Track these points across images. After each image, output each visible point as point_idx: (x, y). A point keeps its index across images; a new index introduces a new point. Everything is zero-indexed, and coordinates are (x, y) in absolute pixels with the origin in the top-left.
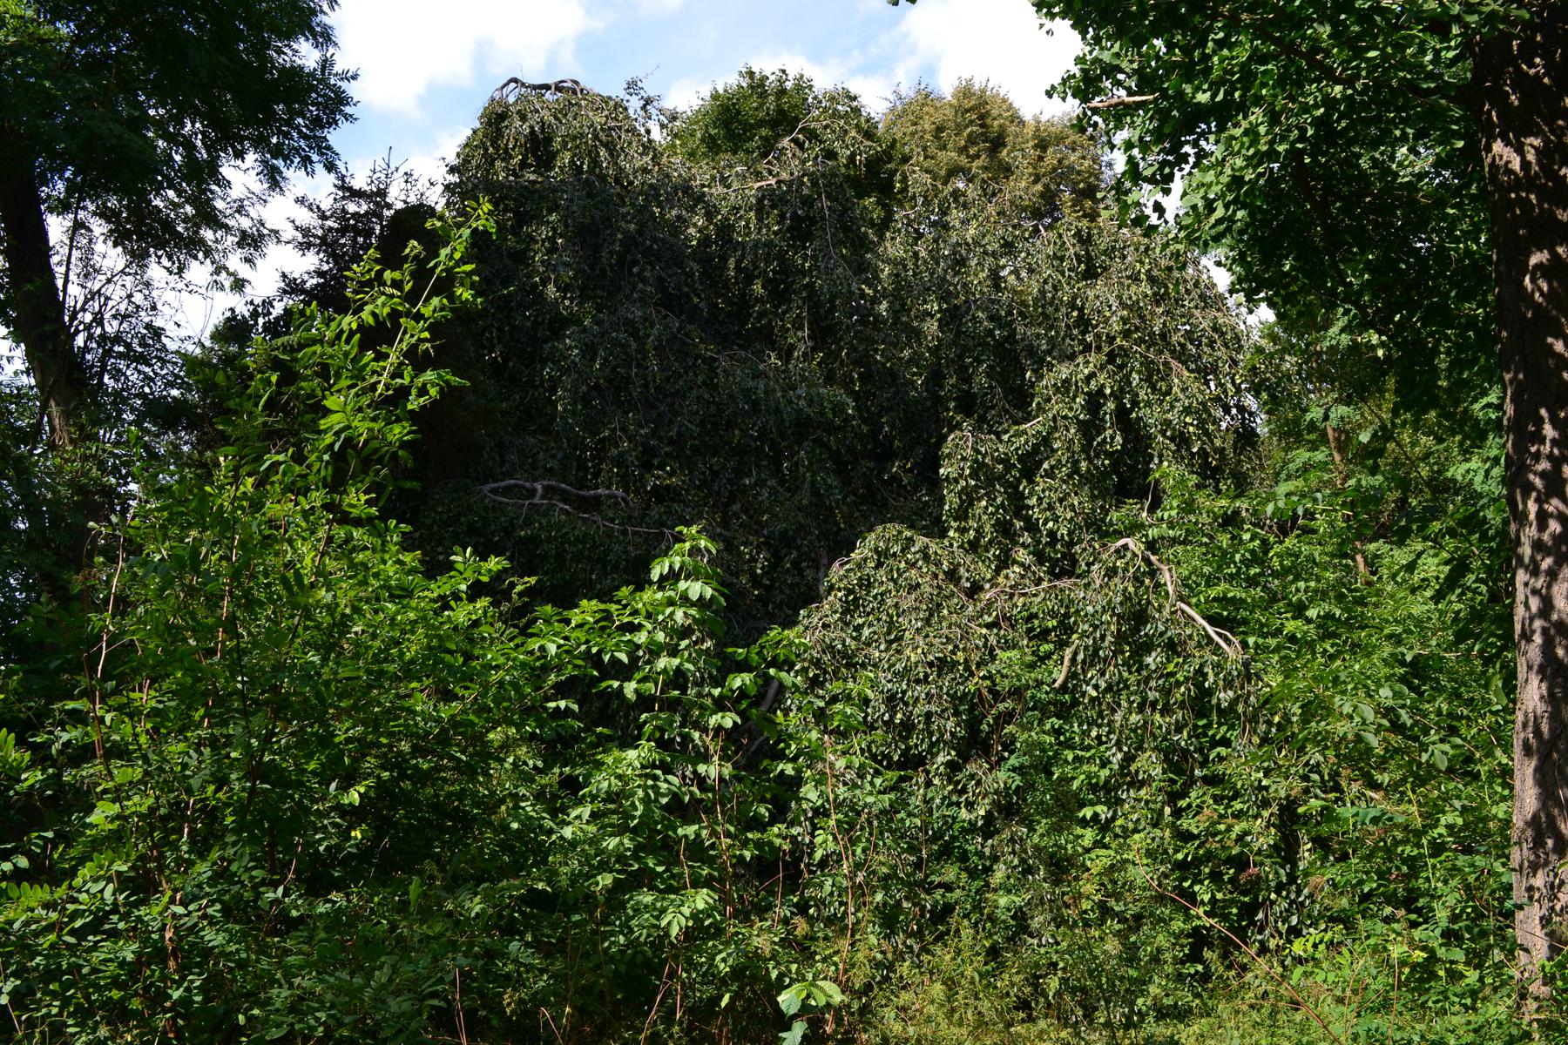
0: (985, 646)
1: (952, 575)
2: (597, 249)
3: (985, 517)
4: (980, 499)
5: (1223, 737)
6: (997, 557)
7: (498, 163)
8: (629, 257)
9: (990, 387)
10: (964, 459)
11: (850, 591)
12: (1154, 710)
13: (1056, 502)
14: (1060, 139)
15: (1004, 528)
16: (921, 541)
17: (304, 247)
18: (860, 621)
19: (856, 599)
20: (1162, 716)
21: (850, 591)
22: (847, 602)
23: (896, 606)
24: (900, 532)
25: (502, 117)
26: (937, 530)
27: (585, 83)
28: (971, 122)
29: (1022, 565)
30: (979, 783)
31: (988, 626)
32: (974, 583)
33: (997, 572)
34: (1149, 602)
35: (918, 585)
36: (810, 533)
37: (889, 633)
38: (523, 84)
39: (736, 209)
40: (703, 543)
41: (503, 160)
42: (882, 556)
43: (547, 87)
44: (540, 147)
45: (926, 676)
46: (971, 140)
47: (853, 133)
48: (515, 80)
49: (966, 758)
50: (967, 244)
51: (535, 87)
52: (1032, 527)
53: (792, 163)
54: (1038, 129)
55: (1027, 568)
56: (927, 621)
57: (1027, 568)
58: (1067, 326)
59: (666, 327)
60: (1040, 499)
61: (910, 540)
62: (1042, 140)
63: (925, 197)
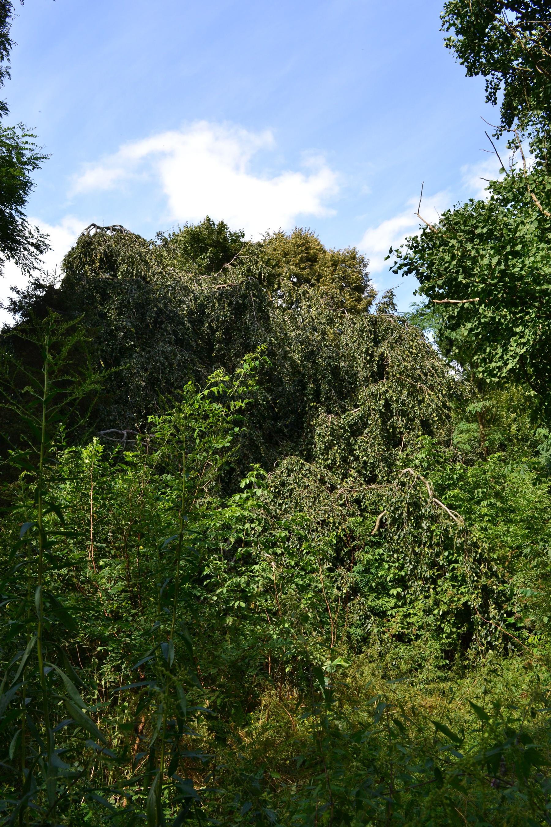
0: (341, 515)
1: (322, 481)
2: (144, 314)
3: (337, 455)
4: (334, 446)
5: (455, 559)
6: (343, 474)
7: (87, 267)
8: (159, 320)
9: (329, 389)
10: (327, 427)
11: (276, 488)
12: (424, 547)
13: (368, 446)
14: (343, 262)
15: (344, 459)
16: (307, 465)
17: (15, 311)
18: (281, 501)
19: (279, 492)
20: (428, 548)
21: (276, 488)
22: (275, 492)
23: (300, 495)
24: (298, 461)
25: (90, 244)
26: (310, 458)
27: (126, 227)
28: (302, 251)
29: (353, 477)
30: (343, 578)
31: (341, 505)
32: (332, 485)
33: (342, 480)
34: (420, 498)
35: (308, 485)
36: (249, 458)
37: (296, 508)
38: (98, 228)
39: (207, 298)
40: (262, 472)
41: (89, 265)
42: (290, 471)
43: (108, 228)
44: (109, 262)
45: (317, 529)
46: (302, 260)
47: (261, 263)
48: (94, 225)
49: (336, 566)
50: (312, 318)
51: (102, 229)
52: (357, 459)
53: (233, 276)
54: (333, 256)
55: (356, 479)
56: (314, 502)
57: (356, 479)
58: (365, 363)
59: (182, 356)
60: (360, 446)
61: (303, 464)
62: (335, 261)
63: (290, 293)
